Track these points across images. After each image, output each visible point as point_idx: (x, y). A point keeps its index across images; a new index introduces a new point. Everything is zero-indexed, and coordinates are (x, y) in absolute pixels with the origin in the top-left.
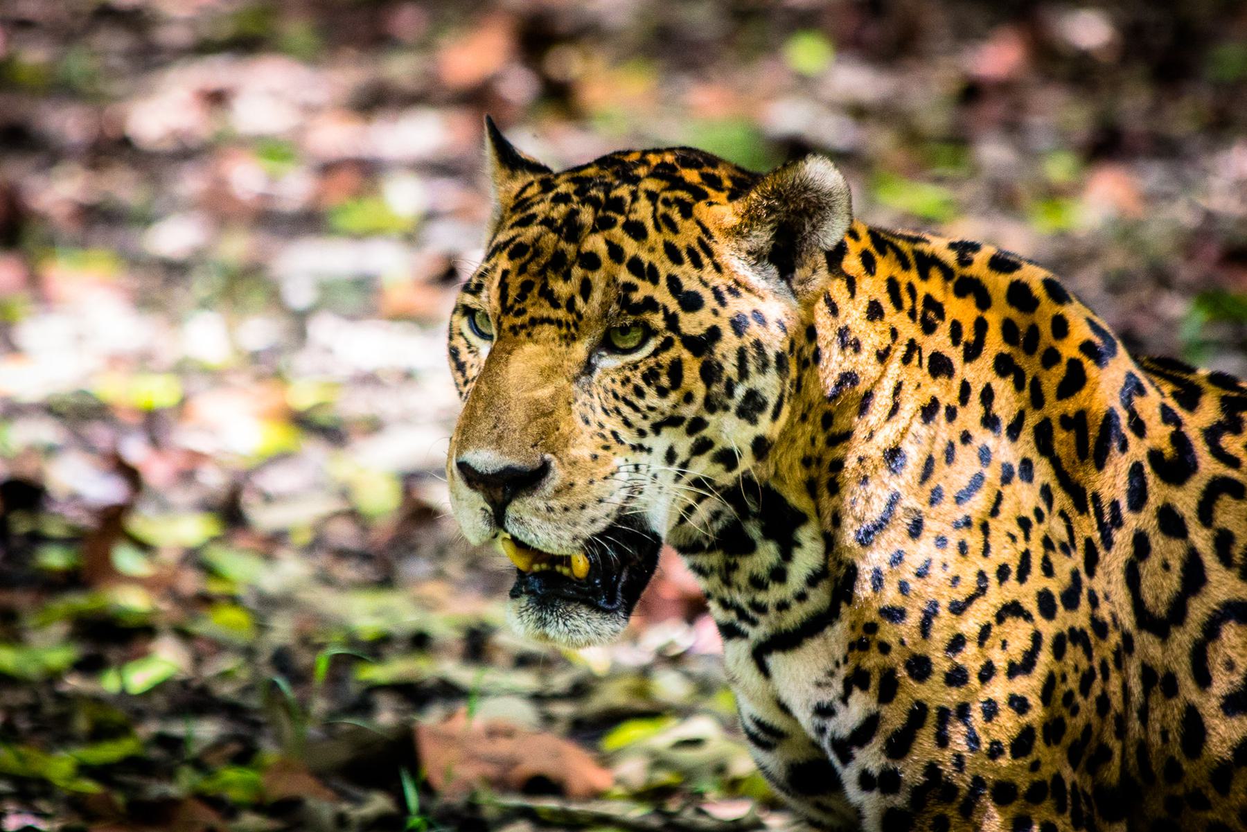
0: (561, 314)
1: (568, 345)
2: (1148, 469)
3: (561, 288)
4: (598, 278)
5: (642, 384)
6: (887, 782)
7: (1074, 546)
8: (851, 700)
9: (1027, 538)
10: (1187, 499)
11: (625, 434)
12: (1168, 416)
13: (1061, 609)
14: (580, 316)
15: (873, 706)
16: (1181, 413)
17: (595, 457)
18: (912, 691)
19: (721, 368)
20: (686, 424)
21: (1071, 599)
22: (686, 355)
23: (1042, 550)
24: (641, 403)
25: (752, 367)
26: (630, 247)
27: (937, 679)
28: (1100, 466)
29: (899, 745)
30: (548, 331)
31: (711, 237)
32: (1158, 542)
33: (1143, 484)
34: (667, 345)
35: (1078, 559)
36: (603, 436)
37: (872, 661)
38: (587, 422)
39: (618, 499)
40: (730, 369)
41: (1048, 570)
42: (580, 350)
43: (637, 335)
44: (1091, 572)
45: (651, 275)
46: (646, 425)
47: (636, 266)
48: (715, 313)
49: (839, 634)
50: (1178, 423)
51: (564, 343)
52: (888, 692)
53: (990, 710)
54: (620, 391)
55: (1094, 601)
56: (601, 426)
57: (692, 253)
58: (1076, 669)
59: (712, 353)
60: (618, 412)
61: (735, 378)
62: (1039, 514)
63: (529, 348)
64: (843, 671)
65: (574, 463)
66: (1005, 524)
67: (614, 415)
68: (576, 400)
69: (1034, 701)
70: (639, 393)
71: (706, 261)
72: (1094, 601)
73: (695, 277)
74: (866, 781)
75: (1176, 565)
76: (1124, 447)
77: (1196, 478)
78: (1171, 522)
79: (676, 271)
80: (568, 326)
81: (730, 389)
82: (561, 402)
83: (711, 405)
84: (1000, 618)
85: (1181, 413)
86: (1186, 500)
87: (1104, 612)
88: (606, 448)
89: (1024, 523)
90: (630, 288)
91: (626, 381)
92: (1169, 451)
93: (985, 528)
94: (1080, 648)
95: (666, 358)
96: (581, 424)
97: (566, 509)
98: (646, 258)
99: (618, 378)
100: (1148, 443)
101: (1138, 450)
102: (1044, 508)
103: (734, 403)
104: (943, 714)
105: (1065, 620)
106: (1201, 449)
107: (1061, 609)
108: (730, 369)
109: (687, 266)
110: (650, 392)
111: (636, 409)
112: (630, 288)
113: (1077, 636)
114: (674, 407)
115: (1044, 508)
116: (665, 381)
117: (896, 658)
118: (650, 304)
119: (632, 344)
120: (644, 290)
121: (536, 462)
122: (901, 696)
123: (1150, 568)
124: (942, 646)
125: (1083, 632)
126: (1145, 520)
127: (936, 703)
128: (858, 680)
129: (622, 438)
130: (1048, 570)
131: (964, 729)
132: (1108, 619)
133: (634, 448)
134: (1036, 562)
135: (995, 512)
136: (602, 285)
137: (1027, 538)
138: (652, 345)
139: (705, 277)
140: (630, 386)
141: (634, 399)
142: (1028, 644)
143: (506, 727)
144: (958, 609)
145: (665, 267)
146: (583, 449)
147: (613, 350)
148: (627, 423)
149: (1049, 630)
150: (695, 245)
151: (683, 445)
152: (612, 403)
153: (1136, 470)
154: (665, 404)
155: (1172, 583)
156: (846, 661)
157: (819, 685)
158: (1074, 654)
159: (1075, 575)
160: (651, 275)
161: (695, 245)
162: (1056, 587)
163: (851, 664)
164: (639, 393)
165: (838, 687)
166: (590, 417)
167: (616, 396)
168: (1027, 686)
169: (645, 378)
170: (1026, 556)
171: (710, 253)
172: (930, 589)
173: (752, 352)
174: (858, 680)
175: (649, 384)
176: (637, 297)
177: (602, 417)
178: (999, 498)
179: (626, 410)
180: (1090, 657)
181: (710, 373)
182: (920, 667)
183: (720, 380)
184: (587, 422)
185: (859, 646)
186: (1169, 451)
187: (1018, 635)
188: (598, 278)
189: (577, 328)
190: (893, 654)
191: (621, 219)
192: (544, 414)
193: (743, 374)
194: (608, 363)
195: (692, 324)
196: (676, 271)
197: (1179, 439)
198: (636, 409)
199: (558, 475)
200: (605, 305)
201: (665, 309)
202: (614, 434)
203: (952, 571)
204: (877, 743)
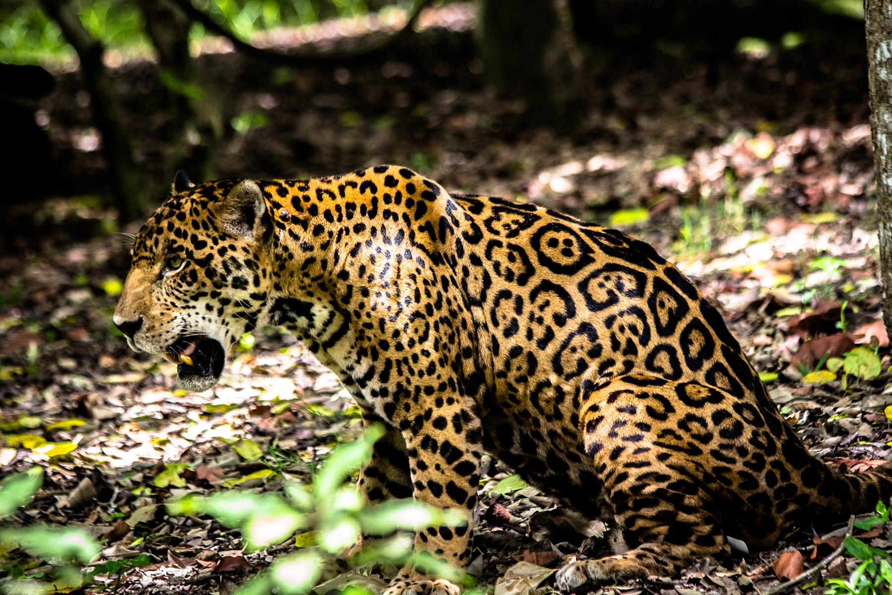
0: (147, 254)
2: (462, 240)
3: (149, 243)
4: (161, 238)
6: (384, 392)
7: (437, 281)
8: (362, 362)
9: (415, 282)
10: (481, 250)
11: (177, 303)
12: (468, 217)
13: (435, 310)
14: (154, 254)
15: (371, 362)
16: (474, 216)
17: (162, 314)
18: (384, 355)
20: (209, 294)
21: (439, 306)
22: (197, 267)
23: (424, 286)
24: (181, 289)
25: (232, 268)
26: (177, 224)
27: (392, 349)
28: (444, 242)
29: (384, 377)
30: (143, 263)
32: (472, 269)
33: (462, 246)
34: (188, 264)
35: (439, 286)
36: (166, 305)
37: (366, 344)
38: (159, 300)
39: (177, 331)
40: (220, 270)
41: (428, 294)
42: (157, 269)
43: (179, 261)
44: (446, 290)
45: (184, 235)
46: (187, 298)
48: (212, 248)
49: (351, 334)
50: (472, 219)
52: (375, 357)
53: (415, 358)
54: (173, 285)
55: (449, 302)
56: (166, 300)
57: (204, 223)
58: (445, 334)
59: (209, 265)
60: (173, 293)
61: (225, 273)
62: (418, 271)
63: (137, 271)
64: (356, 350)
65: (154, 317)
66: (405, 280)
67: (171, 295)
68: (154, 291)
69: (432, 351)
71: (210, 226)
72: (449, 302)
73: (204, 234)
74: (374, 394)
75: (480, 277)
76: (452, 232)
77: (483, 240)
78: (475, 260)
79: (197, 232)
81: (223, 278)
82: (147, 293)
83: (217, 285)
85: (474, 216)
86: (480, 250)
87: (454, 307)
88: (169, 309)
89: (413, 277)
90: (174, 242)
91: (175, 281)
92: (471, 232)
93: (395, 283)
94: (445, 325)
95: (188, 270)
96: (155, 301)
98: (183, 228)
99: (172, 280)
100: (461, 229)
101: (458, 233)
102: (420, 267)
104: (398, 362)
105: (437, 315)
106: (483, 228)
107: (435, 310)
108: (220, 270)
109: (201, 230)
110: (184, 284)
111: (180, 292)
113: (444, 320)
114: (198, 288)
115: (420, 267)
116: (189, 279)
117: (374, 342)
118: (181, 248)
119: (178, 265)
122: (380, 357)
123: (470, 280)
124: (391, 335)
125: (446, 318)
126: (465, 261)
127: (395, 358)
128: (362, 353)
129: (177, 304)
130: (428, 294)
131: (407, 367)
132: (456, 308)
133: (184, 308)
134: (422, 291)
135: (398, 276)
136: (163, 241)
137: (415, 282)
138: (184, 264)
139: (209, 233)
141: (178, 288)
142: (424, 328)
143: (33, 531)
144: (393, 320)
145: (191, 231)
146: (156, 312)
147: (172, 268)
149: (431, 321)
150: (206, 220)
152: (170, 291)
153: (458, 242)
154: (194, 288)
155: (480, 283)
156: (356, 345)
157: (346, 358)
158: (443, 328)
159: (439, 294)
160: (184, 235)
161: (206, 220)
162: (432, 302)
163: (358, 346)
164: (181, 286)
165: (354, 356)
166: (161, 297)
167: (172, 287)
168: (429, 345)
169: (181, 279)
170: (417, 291)
171: (212, 223)
172: (379, 314)
173: (229, 263)
174: (362, 353)
176: (175, 246)
177: (166, 297)
178: (399, 269)
179: (176, 293)
180: (451, 327)
181: (211, 273)
182: (385, 345)
183: (216, 275)
184: (159, 300)
185: (361, 337)
186: (471, 232)
188: (161, 238)
189: (154, 259)
190: (372, 341)
191: (177, 212)
192: (140, 298)
193: (229, 272)
194: (169, 274)
195: (199, 254)
196: (197, 232)
197: (474, 226)
199: (146, 324)
200: (163, 249)
201: (187, 249)
202: (172, 303)
203: (387, 305)
204: (376, 377)
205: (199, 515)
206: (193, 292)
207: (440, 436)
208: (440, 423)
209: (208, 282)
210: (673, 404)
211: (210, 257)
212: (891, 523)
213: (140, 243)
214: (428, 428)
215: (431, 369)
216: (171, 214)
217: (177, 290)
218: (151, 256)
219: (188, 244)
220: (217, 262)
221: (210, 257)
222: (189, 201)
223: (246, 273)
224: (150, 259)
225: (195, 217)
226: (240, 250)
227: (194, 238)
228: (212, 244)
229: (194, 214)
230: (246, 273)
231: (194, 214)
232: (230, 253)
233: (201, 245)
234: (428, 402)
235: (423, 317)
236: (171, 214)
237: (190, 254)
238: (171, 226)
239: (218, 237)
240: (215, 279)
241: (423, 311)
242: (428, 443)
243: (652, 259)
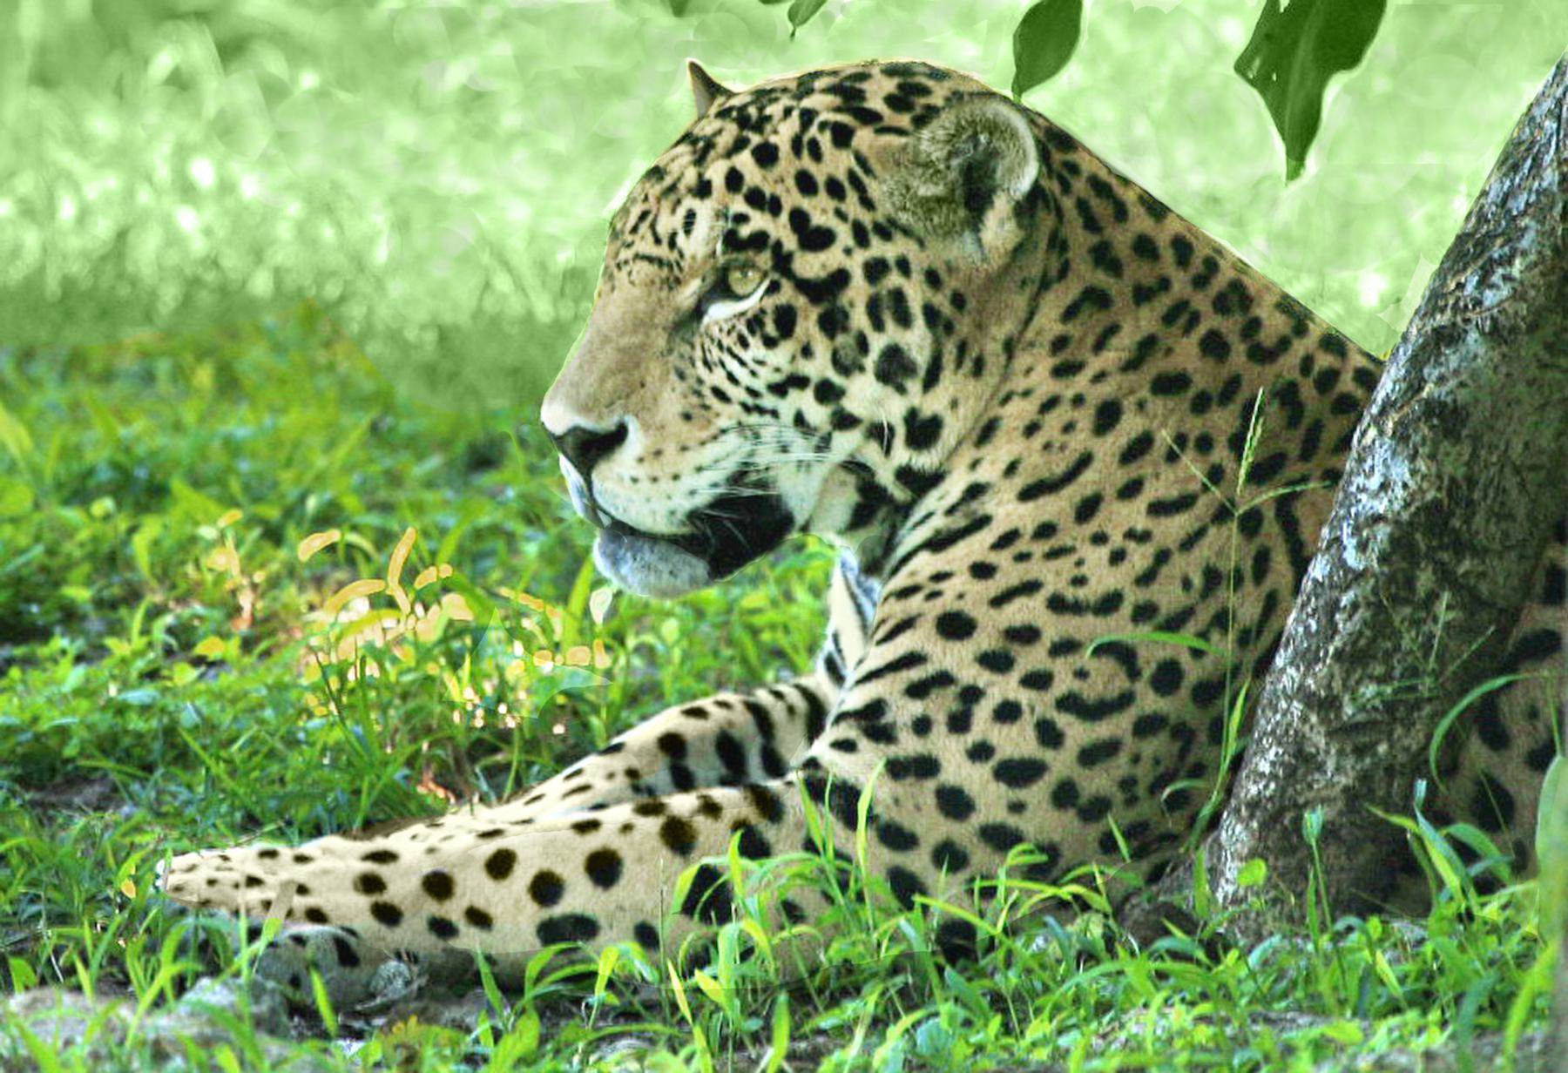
1: (671, 289)
5: (745, 332)
19: (846, 316)
22: (801, 301)
24: (747, 356)
26: (752, 174)
31: (868, 171)
34: (774, 288)
46: (759, 385)
47: (756, 198)
48: (848, 252)
51: (666, 287)
60: (723, 364)
70: (744, 343)
79: (806, 203)
80: (670, 266)
83: (845, 367)
84: (1100, 651)
90: (741, 219)
97: (655, 480)
103: (870, 361)
110: (755, 342)
111: (742, 363)
112: (741, 219)
116: (770, 329)
119: (749, 288)
120: (759, 221)
121: (608, 424)
140: (734, 335)
141: (738, 350)
145: (792, 198)
148: (732, 378)
151: (818, 415)
160: (774, 207)
164: (744, 343)
166: (689, 371)
175: (752, 332)
176: (745, 231)
179: (733, 365)
183: (845, 329)
187: (1104, 679)
195: (811, 265)
196: (806, 203)
198: (742, 363)
205: (93, 792)
206: (777, 370)
209: (822, 347)
210: (484, 980)
211: (840, 278)
212: (1339, 1068)
213: (643, 216)
216: (739, 145)
217: (735, 356)
218: (674, 256)
219: (780, 229)
221: (840, 278)
222: (795, 114)
224: (670, 266)
225: (806, 162)
226: (917, 276)
227: (799, 220)
228: (850, 242)
229: (805, 153)
231: (805, 153)
232: (894, 279)
233: (817, 239)
235: (1134, 674)
236: (739, 145)
237: (782, 262)
238: (734, 180)
239: (869, 227)
240: (841, 339)
241: (1148, 663)
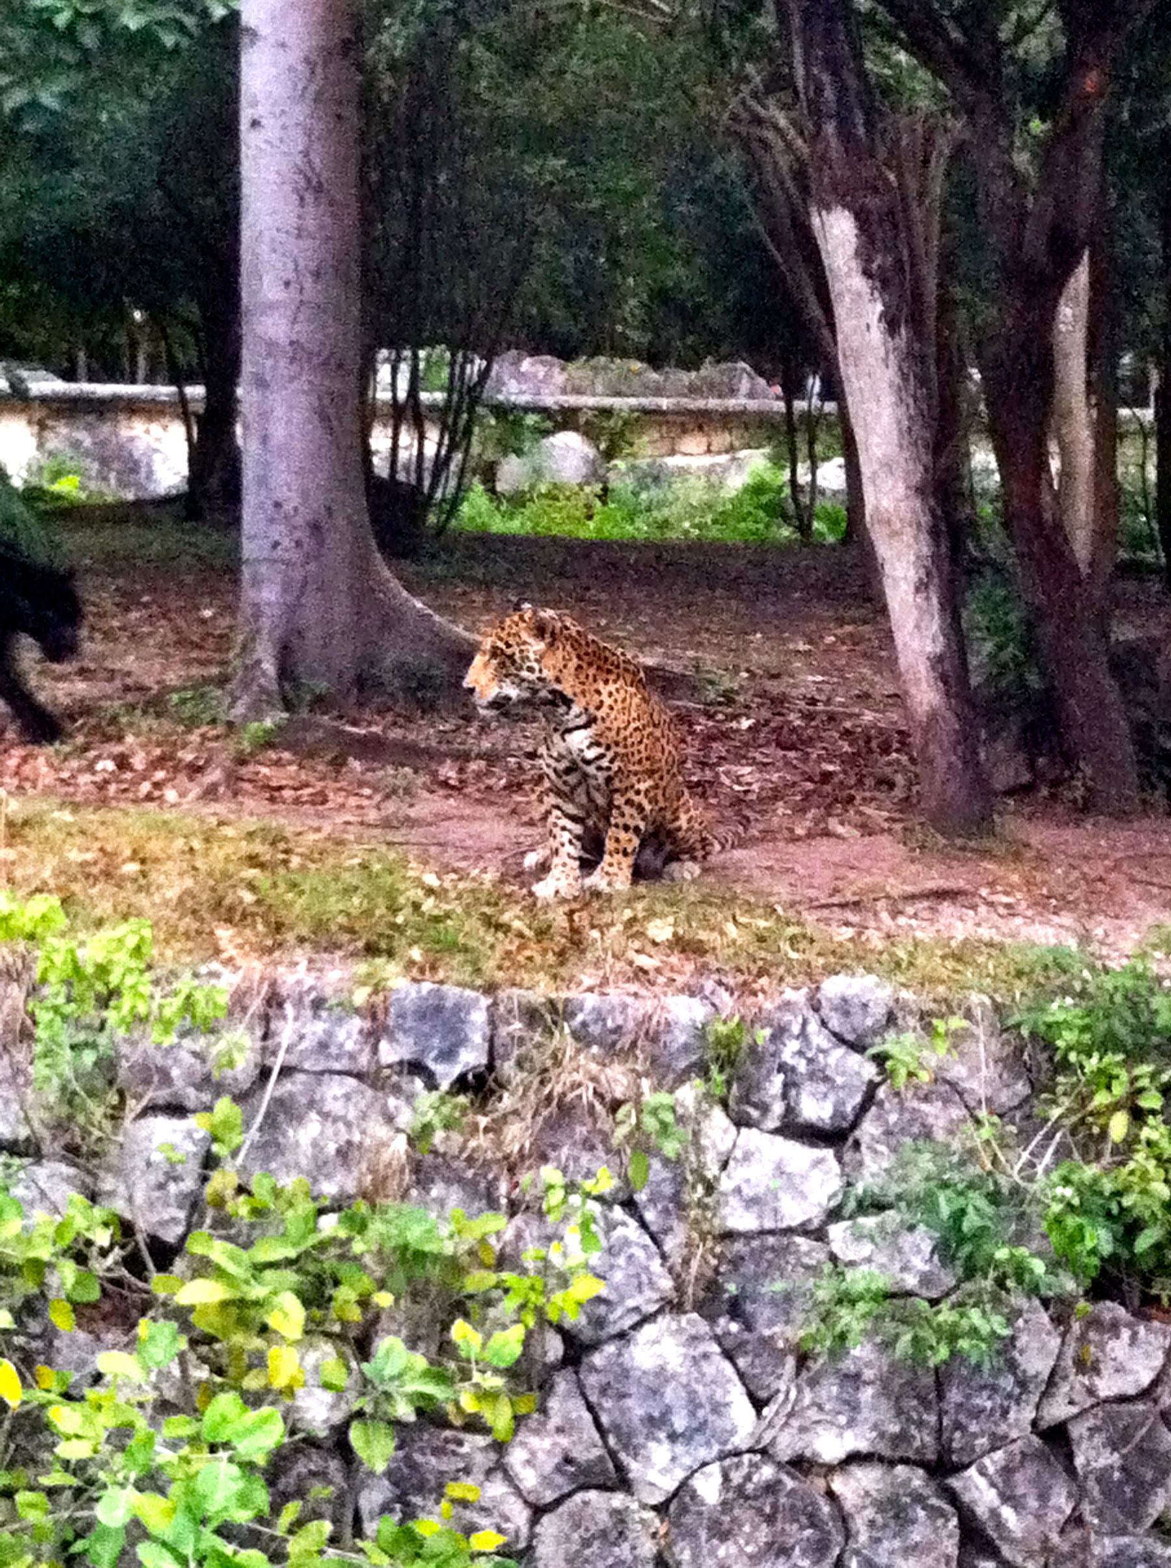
52: (608, 748)
207: (636, 799)
208: (638, 793)
214: (631, 794)
215: (640, 762)
220: (517, 656)
223: (536, 666)
230: (536, 666)
234: (634, 779)
242: (629, 802)
243: (1091, 258)
